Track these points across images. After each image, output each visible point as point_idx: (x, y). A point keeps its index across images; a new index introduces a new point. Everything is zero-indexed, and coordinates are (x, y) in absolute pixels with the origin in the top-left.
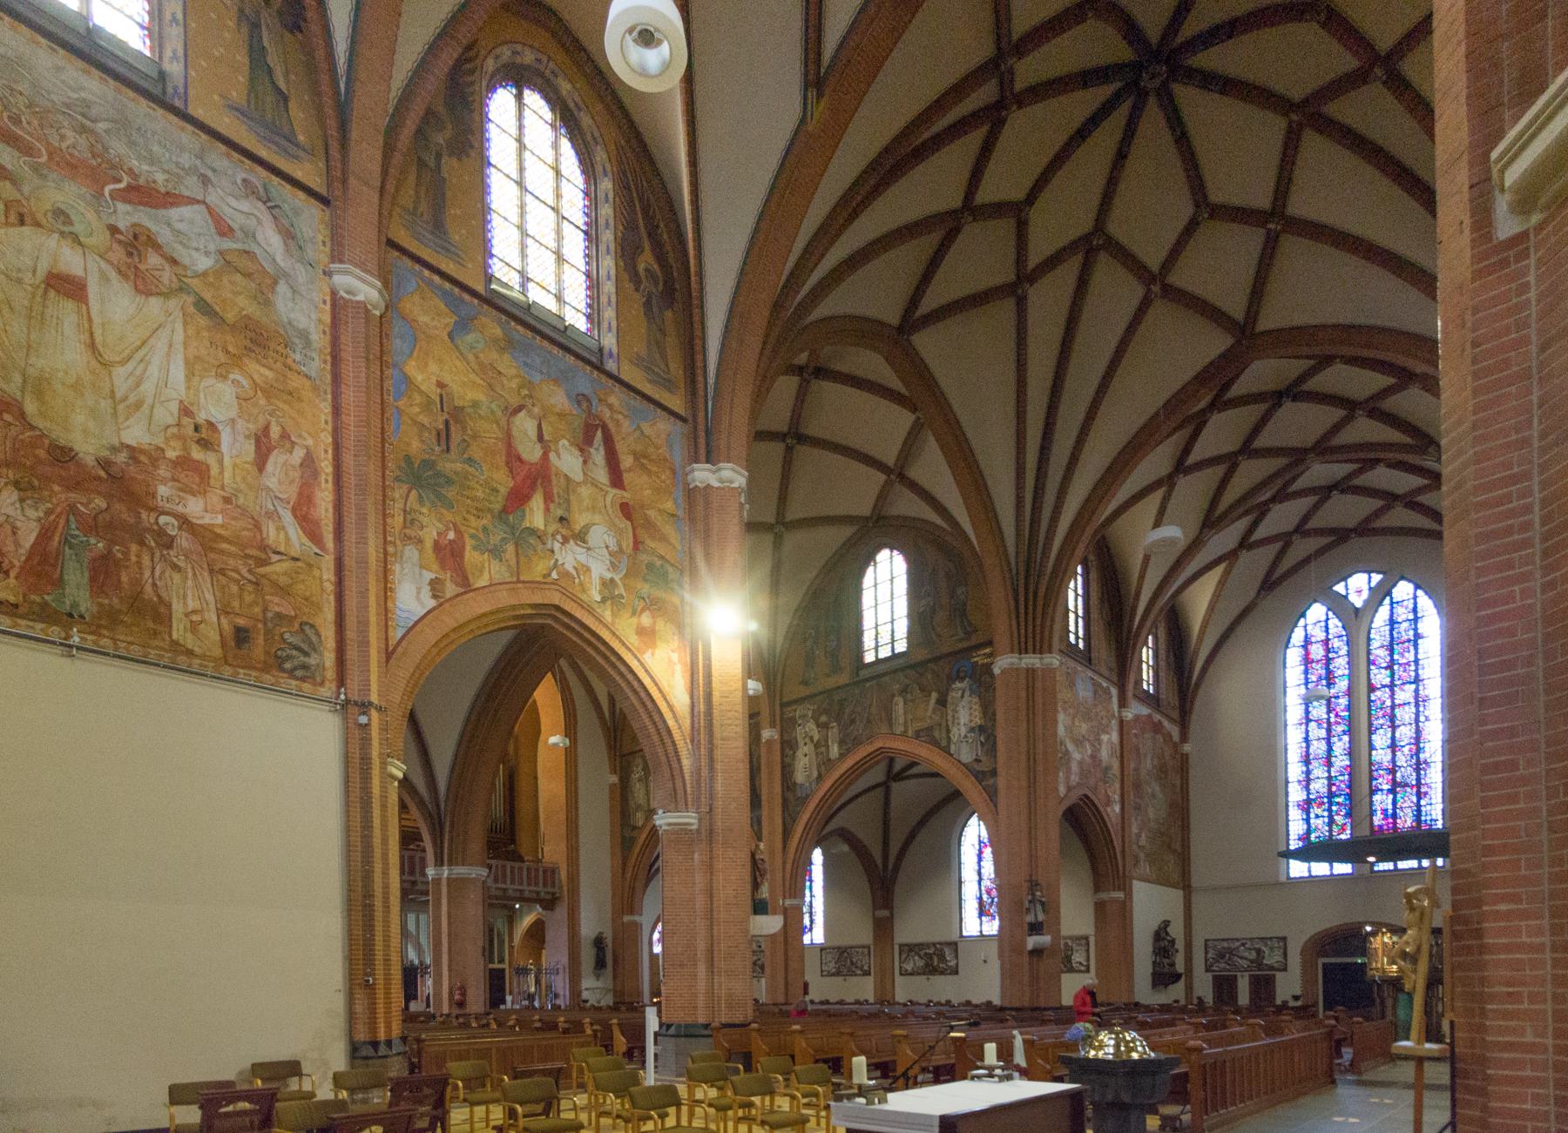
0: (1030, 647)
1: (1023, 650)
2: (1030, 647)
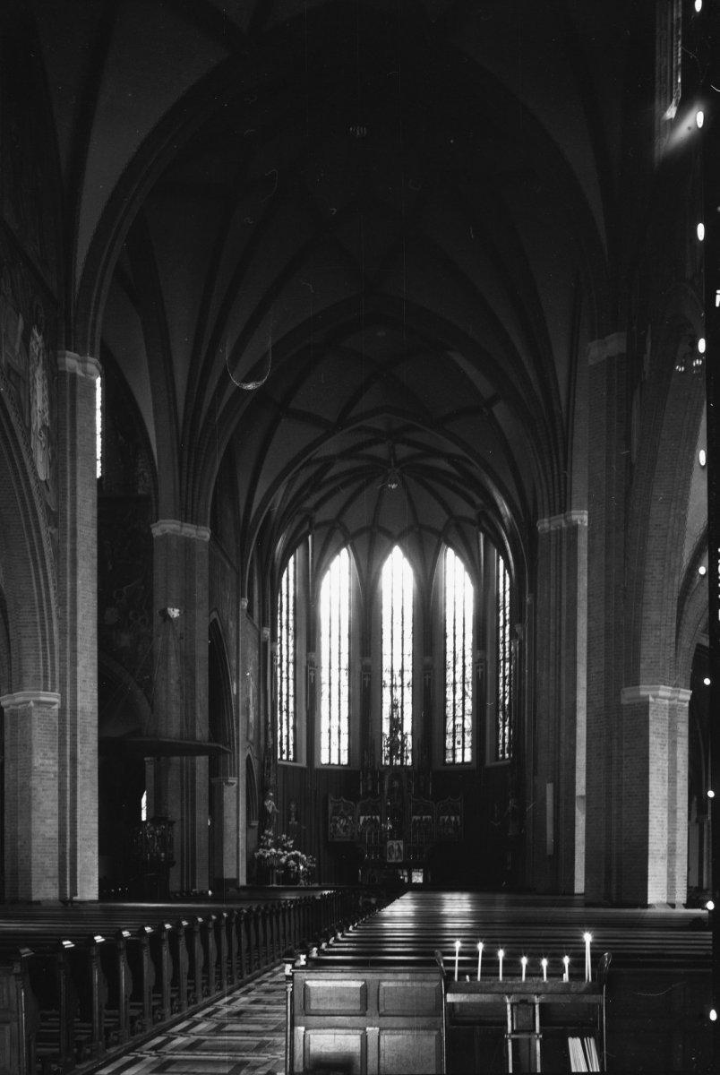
0: (557, 511)
1: (552, 513)
2: (557, 511)
